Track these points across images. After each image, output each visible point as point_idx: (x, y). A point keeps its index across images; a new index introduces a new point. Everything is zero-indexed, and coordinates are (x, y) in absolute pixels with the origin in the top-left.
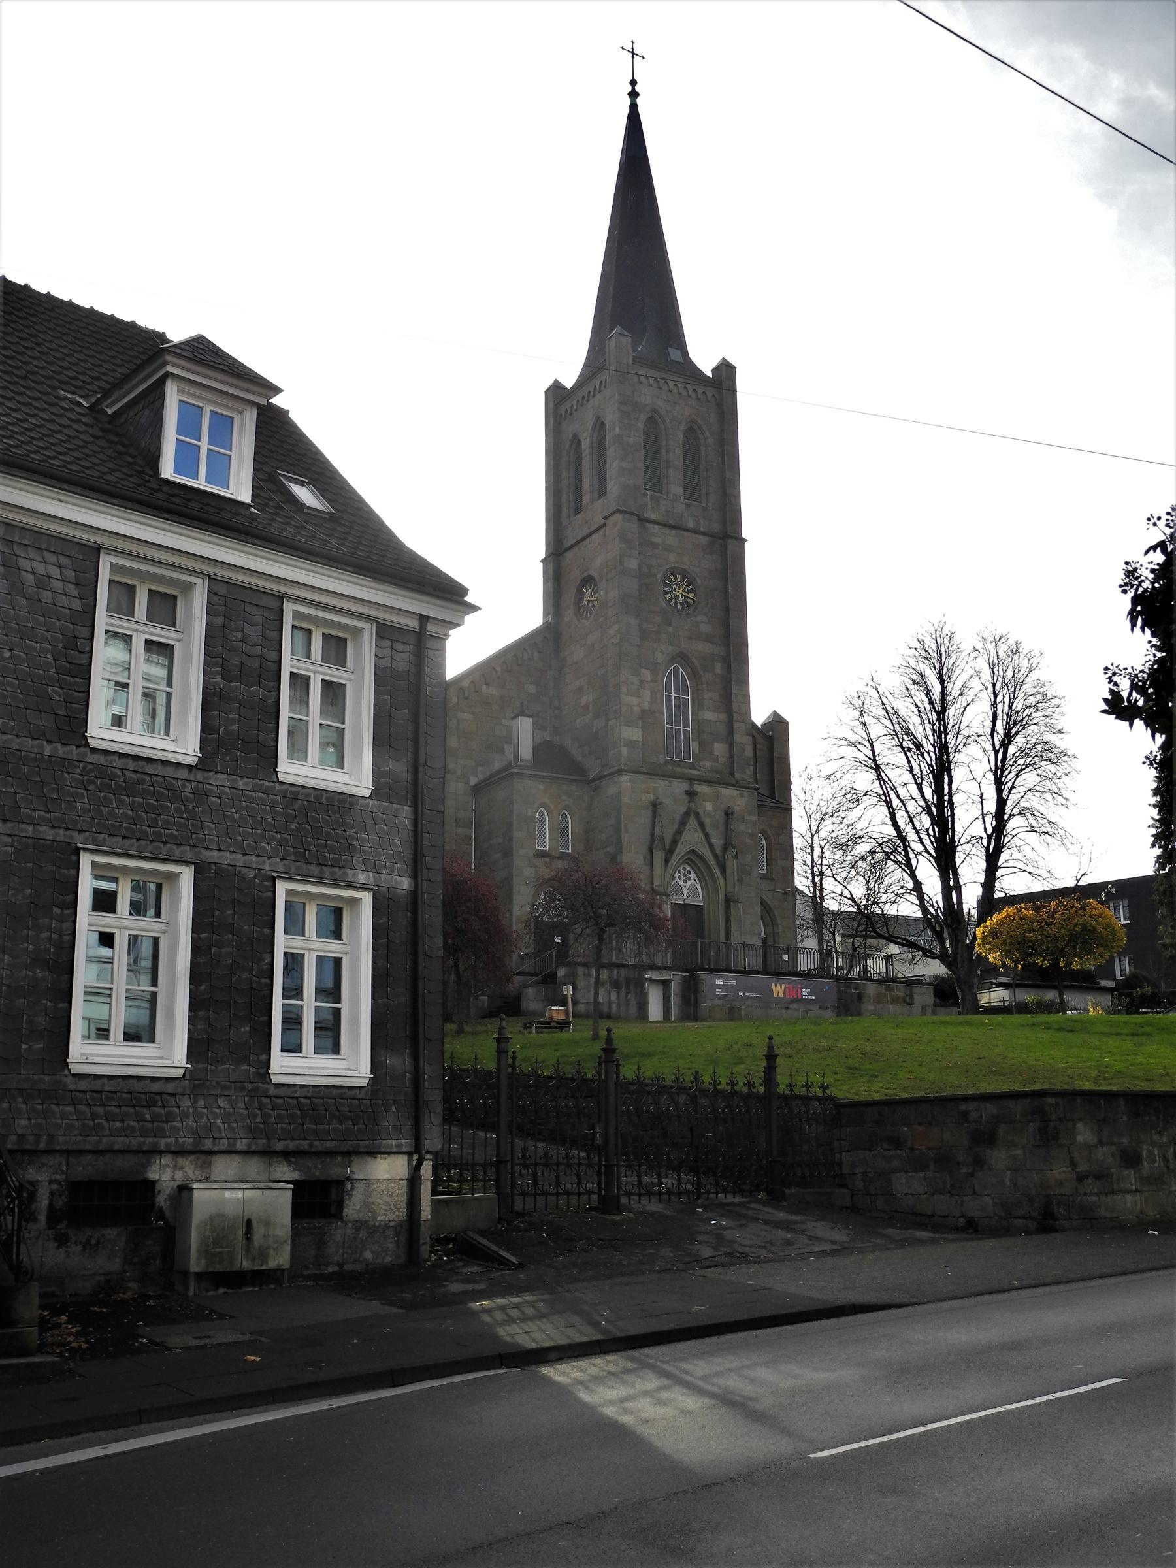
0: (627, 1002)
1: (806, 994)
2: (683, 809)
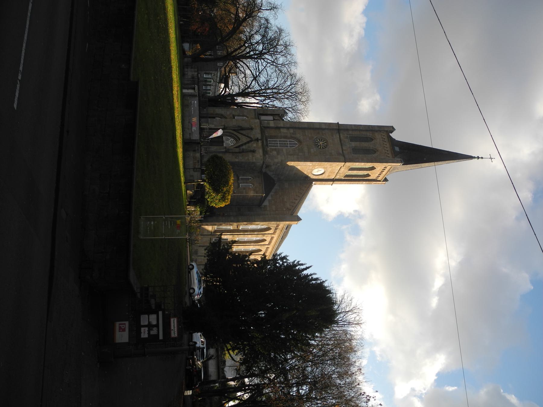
1: (194, 128)
2: (252, 136)
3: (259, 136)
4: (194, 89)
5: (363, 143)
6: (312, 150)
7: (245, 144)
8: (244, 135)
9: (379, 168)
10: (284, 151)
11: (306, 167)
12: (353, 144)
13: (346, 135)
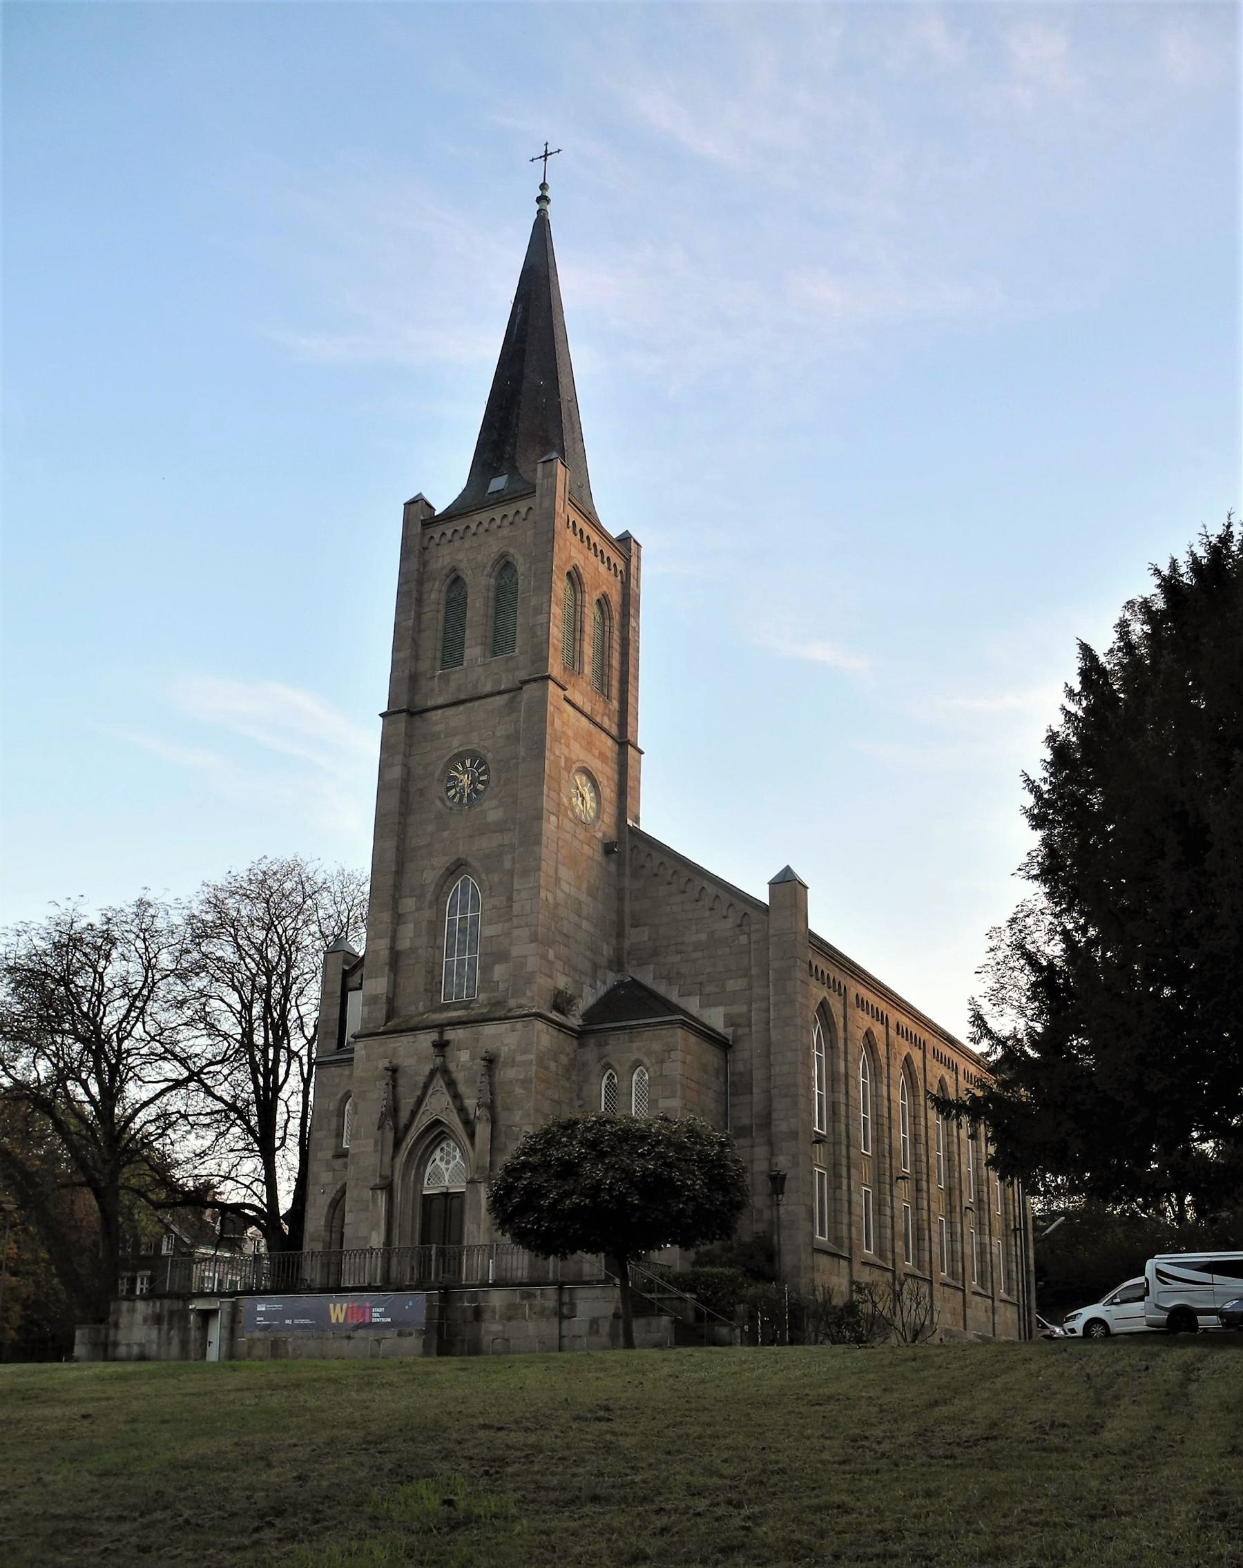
0: (169, 1341)
3: (426, 1040)
6: (493, 816)
7: (456, 1097)
8: (420, 1101)
9: (574, 553)
10: (490, 931)
11: (566, 870)
12: (473, 652)
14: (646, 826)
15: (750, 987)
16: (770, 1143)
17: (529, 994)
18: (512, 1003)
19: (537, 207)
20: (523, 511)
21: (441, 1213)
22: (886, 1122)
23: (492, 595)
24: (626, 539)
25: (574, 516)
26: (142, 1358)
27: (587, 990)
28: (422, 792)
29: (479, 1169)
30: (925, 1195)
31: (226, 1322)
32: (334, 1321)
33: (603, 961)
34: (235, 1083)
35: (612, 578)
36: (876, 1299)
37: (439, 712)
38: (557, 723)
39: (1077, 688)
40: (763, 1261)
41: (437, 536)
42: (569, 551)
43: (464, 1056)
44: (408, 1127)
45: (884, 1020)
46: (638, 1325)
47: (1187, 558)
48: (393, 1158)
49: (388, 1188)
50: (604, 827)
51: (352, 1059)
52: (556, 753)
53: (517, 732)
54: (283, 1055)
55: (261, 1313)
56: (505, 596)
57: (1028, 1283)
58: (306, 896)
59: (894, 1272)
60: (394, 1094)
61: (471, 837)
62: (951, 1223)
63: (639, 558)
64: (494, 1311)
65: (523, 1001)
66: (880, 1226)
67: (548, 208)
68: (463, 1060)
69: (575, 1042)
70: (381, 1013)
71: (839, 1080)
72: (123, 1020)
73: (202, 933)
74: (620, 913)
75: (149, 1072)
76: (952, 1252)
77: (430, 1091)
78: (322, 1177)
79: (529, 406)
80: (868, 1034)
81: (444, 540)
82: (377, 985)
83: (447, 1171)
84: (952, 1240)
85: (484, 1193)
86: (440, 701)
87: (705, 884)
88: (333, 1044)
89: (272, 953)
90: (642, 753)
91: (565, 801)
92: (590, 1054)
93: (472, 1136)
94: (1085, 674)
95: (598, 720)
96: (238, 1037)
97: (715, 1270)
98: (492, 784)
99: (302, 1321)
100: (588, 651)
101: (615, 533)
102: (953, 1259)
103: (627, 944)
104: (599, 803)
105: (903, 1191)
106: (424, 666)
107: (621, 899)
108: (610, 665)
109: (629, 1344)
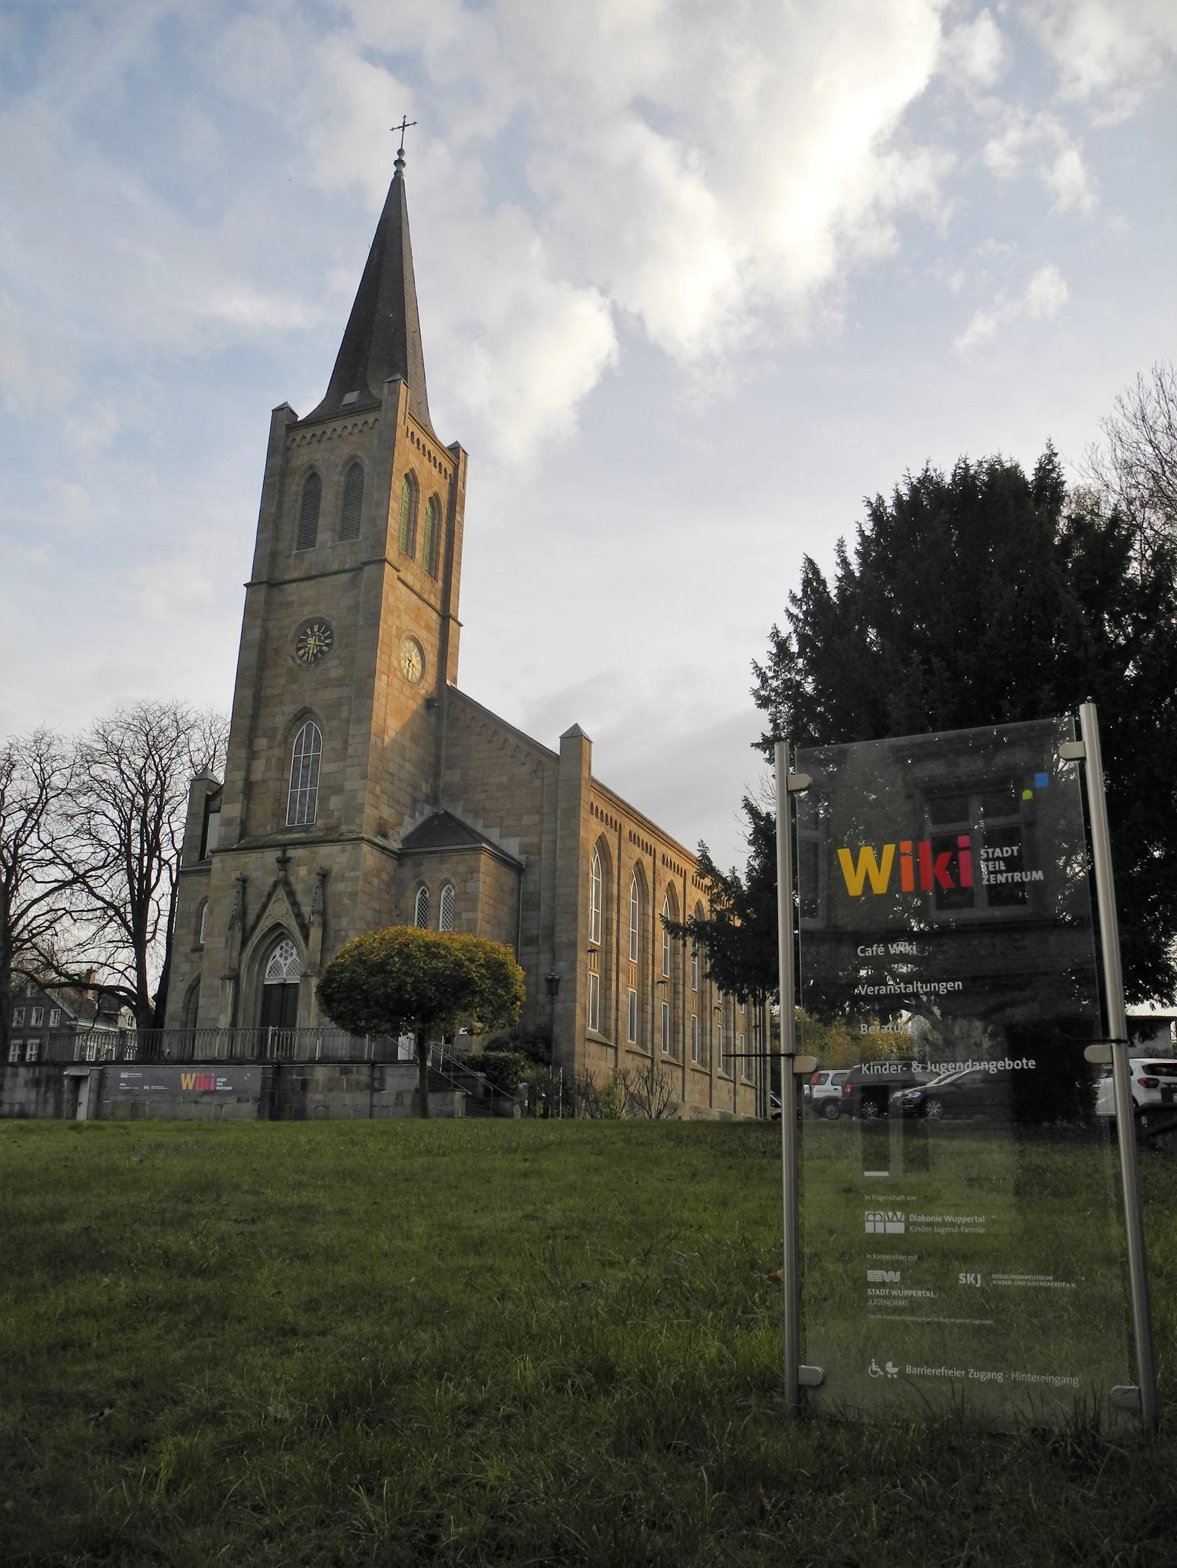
0: (46, 1101)
1: (220, 1084)
2: (271, 880)
3: (271, 856)
4: (78, 1081)
5: (322, 505)
6: (335, 673)
7: (295, 904)
8: (264, 907)
12: (324, 536)
13: (292, 561)
14: (461, 687)
15: (542, 822)
16: (553, 951)
17: (358, 821)
18: (344, 828)
19: (395, 169)
20: (371, 421)
21: (278, 1004)
22: (650, 936)
23: (341, 489)
24: (455, 449)
25: (413, 428)
26: (22, 1115)
27: (407, 819)
28: (276, 651)
29: (310, 964)
30: (681, 997)
31: (94, 1086)
32: (184, 1088)
33: (420, 796)
34: (116, 887)
35: (442, 480)
36: (629, 1083)
37: (294, 585)
38: (391, 599)
39: (799, 595)
40: (543, 1044)
41: (298, 439)
42: (406, 457)
43: (303, 871)
44: (253, 928)
45: (651, 852)
46: (433, 1100)
47: (893, 494)
48: (240, 954)
49: (235, 978)
50: (426, 685)
51: (209, 870)
52: (388, 624)
53: (357, 605)
54: (155, 862)
55: (124, 1080)
56: (353, 492)
57: (765, 1070)
58: (180, 732)
59: (652, 1059)
60: (243, 900)
61: (316, 689)
62: (702, 1019)
63: (465, 464)
64: (317, 1084)
65: (352, 828)
66: (643, 1021)
67: (404, 170)
68: (302, 874)
69: (396, 863)
70: (235, 831)
71: (612, 901)
72: (20, 830)
73: (88, 759)
74: (437, 757)
75: (38, 874)
76: (703, 1044)
77: (273, 899)
78: (182, 966)
79: (379, 338)
80: (639, 863)
81: (304, 442)
82: (233, 810)
83: (285, 965)
84: (703, 1034)
85: (314, 982)
86: (296, 575)
87: (509, 736)
88: (196, 855)
89: (150, 778)
90: (461, 625)
91: (395, 663)
92: (407, 872)
93: (306, 937)
94: (807, 583)
95: (426, 597)
96: (118, 847)
97: (502, 1054)
98: (335, 646)
99: (158, 1087)
100: (420, 539)
101: (446, 442)
102: (702, 1049)
103: (442, 784)
104: (423, 665)
105: (662, 992)
106: (283, 546)
107: (438, 745)
108: (438, 553)
109: (424, 1113)
